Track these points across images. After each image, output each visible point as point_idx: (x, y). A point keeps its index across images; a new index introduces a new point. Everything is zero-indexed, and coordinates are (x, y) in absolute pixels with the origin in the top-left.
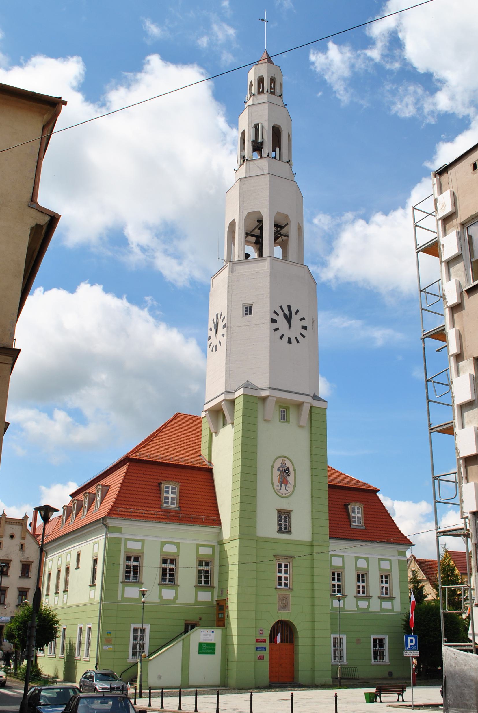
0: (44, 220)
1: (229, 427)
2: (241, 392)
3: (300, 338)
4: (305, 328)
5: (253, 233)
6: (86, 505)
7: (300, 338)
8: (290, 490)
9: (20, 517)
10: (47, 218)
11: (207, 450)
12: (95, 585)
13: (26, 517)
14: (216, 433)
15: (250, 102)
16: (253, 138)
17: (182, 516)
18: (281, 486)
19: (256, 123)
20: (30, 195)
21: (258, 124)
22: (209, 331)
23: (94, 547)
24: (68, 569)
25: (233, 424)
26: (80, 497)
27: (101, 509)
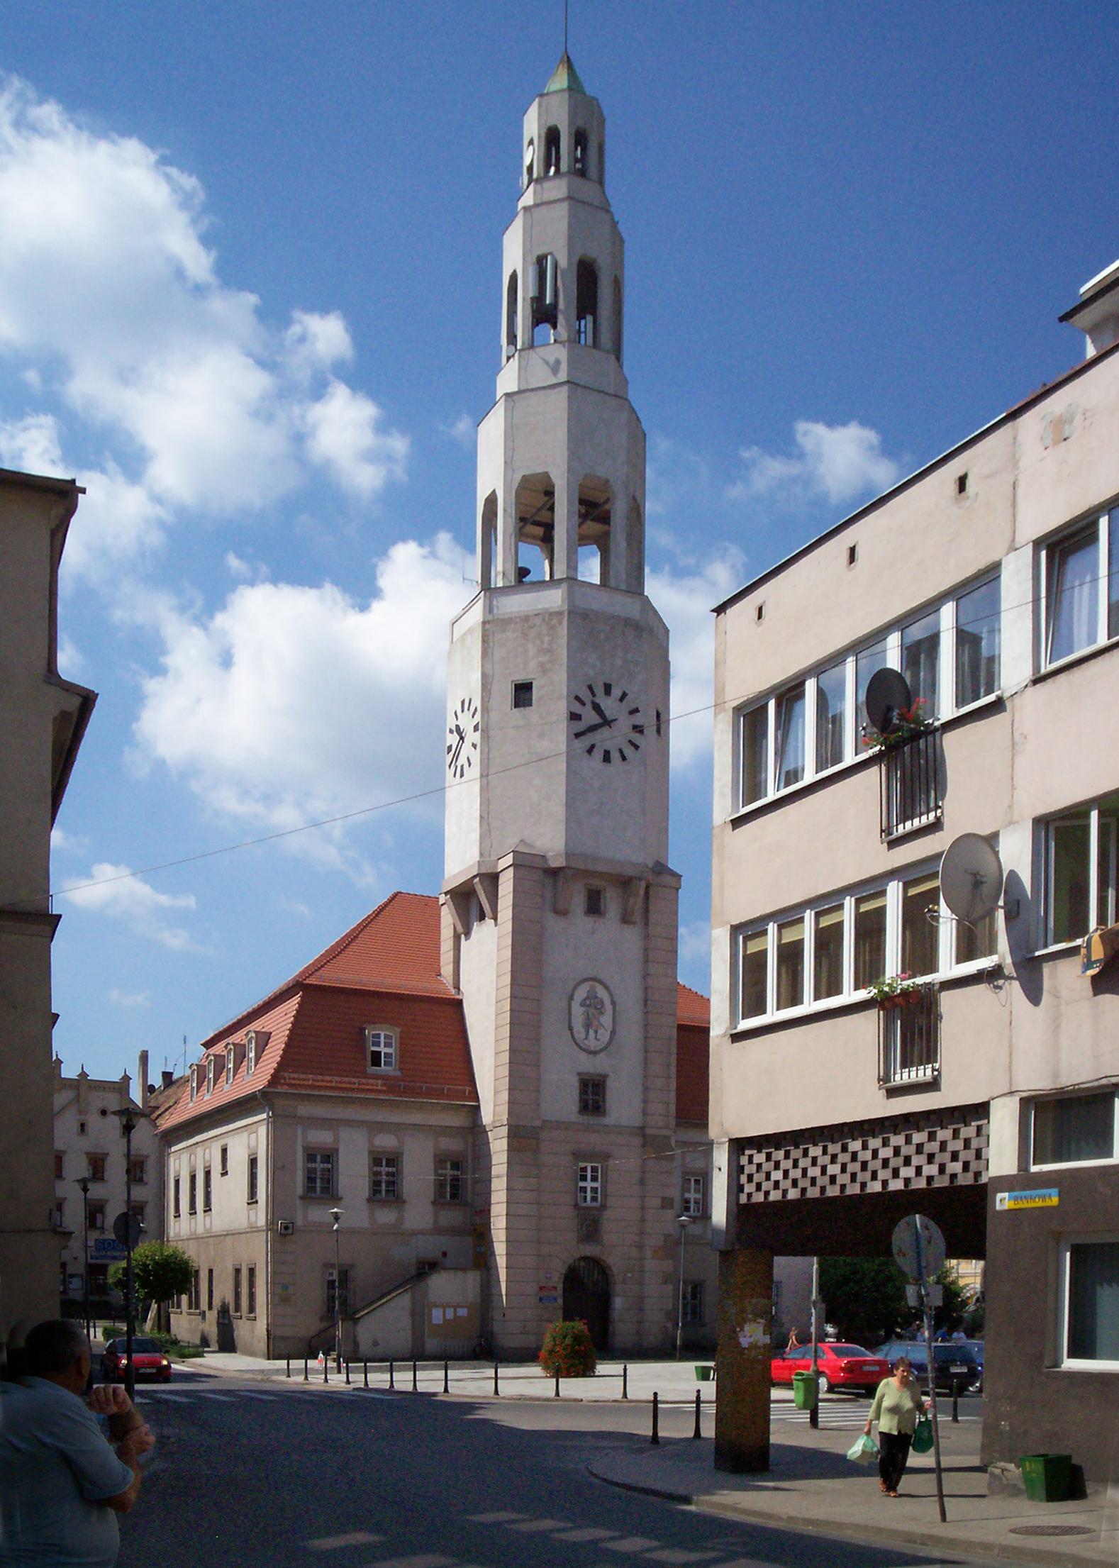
0: (74, 703)
1: (489, 922)
2: (509, 860)
3: (628, 751)
4: (638, 729)
5: (537, 518)
6: (231, 1066)
7: (628, 751)
8: (604, 1036)
9: (116, 1077)
10: (77, 701)
11: (451, 966)
12: (256, 1202)
13: (126, 1079)
14: (468, 934)
15: (528, 199)
16: (532, 292)
17: (407, 1088)
18: (587, 1033)
19: (540, 253)
20: (45, 662)
21: (545, 257)
22: (449, 736)
23: (249, 1139)
24: (208, 1174)
25: (495, 919)
26: (219, 1049)
27: (255, 1077)
